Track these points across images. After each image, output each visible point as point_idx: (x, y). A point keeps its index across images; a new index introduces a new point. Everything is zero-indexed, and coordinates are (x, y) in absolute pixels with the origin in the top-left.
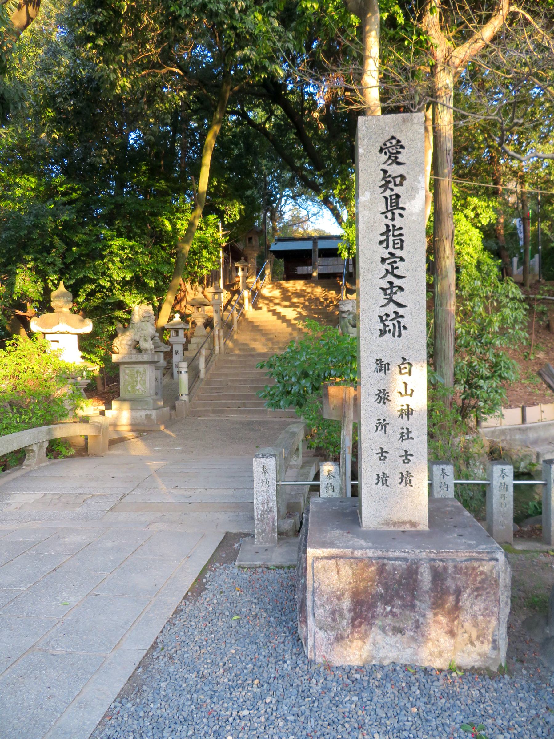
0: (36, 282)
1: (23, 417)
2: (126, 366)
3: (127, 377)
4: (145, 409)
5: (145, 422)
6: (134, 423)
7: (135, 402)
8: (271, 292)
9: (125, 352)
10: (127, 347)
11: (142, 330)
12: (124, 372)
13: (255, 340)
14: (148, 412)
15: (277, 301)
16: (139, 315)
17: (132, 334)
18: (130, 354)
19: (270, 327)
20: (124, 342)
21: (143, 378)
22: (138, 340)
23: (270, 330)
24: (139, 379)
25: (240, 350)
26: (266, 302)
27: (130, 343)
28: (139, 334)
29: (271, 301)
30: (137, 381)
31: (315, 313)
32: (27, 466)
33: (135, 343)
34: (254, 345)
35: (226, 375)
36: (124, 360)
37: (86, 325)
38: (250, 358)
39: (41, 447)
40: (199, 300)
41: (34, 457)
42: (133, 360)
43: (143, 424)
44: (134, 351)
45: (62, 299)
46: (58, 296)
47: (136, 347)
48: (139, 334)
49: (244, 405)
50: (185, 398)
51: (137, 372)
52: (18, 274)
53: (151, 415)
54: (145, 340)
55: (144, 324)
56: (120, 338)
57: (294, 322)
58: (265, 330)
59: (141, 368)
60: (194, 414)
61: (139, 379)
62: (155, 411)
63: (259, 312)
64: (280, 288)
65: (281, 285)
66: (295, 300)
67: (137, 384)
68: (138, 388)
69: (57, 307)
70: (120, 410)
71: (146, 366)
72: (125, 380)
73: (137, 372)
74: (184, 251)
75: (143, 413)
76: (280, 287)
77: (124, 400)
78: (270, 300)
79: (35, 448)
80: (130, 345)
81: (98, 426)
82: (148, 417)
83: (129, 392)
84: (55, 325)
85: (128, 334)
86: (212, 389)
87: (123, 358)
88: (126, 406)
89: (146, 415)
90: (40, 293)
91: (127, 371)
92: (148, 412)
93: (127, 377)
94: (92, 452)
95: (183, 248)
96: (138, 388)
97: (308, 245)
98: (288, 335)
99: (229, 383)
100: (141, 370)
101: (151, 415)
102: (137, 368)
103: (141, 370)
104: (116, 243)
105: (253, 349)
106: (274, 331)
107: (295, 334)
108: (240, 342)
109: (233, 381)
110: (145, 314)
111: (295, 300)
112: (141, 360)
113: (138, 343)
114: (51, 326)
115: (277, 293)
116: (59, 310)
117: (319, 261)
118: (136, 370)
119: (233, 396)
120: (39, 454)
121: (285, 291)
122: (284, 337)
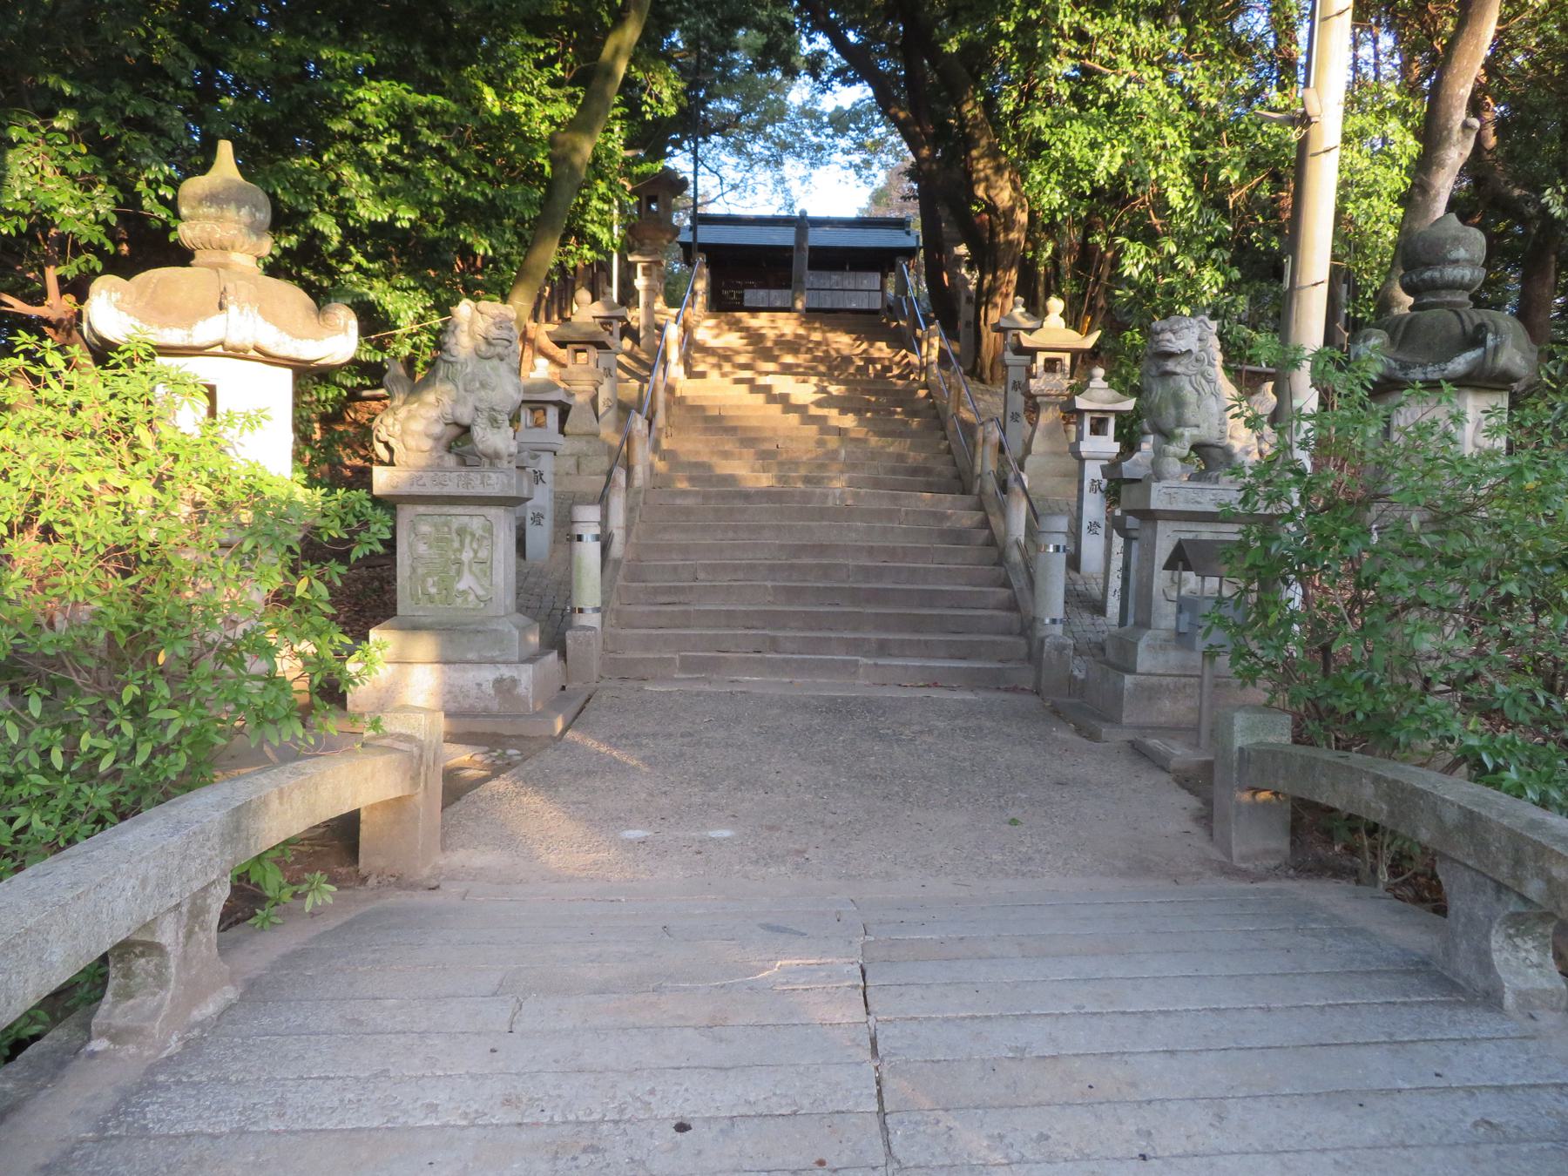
0: (88, 186)
1: (86, 741)
2: (421, 509)
3: (422, 548)
4: (493, 662)
5: (495, 706)
6: (453, 707)
7: (457, 636)
8: (717, 336)
9: (422, 460)
10: (427, 444)
11: (483, 386)
12: (413, 528)
13: (726, 455)
14: (506, 672)
15: (742, 359)
16: (472, 335)
17: (446, 399)
18: (437, 467)
19: (754, 423)
20: (417, 426)
21: (483, 554)
22: (466, 420)
23: (758, 429)
24: (467, 556)
25: (691, 479)
26: (713, 360)
27: (437, 429)
28: (471, 400)
29: (727, 358)
30: (459, 563)
31: (869, 392)
32: (117, 1036)
33: (455, 431)
34: (726, 467)
35: (685, 550)
36: (416, 490)
37: (335, 330)
38: (738, 504)
39: (198, 912)
40: (585, 329)
41: (161, 981)
42: (452, 489)
43: (487, 714)
44: (450, 460)
45: (231, 212)
46: (213, 198)
47: (458, 440)
48: (471, 400)
49: (774, 644)
50: (591, 619)
51: (461, 532)
52: (12, 145)
53: (514, 682)
54: (494, 422)
55: (488, 365)
56: (402, 413)
57: (814, 411)
58: (745, 429)
59: (474, 519)
60: (622, 671)
61: (467, 556)
62: (529, 668)
63: (697, 382)
64: (740, 330)
65: (739, 321)
66: (789, 359)
67: (459, 573)
68: (462, 586)
69: (209, 245)
70: (401, 661)
71: (493, 512)
72: (416, 559)
73: (461, 532)
74: (577, 160)
75: (488, 675)
76: (736, 326)
77: (414, 627)
78: (724, 356)
79: (168, 936)
80: (437, 439)
81: (411, 756)
82: (504, 688)
83: (431, 599)
84: (204, 314)
85: (430, 397)
86: (656, 591)
87: (413, 481)
88: (424, 647)
89: (499, 682)
90: (105, 223)
91: (425, 528)
92: (506, 672)
93: (422, 548)
94: (380, 862)
95: (575, 149)
96: (462, 586)
97: (784, 237)
98: (811, 445)
99: (701, 575)
100: (476, 524)
101: (514, 682)
102: (461, 517)
103: (476, 524)
104: (373, 97)
105: (730, 479)
106: (767, 434)
107: (833, 442)
108: (684, 458)
109: (712, 569)
110: (494, 332)
111: (789, 359)
112: (478, 490)
113: (466, 430)
114: (189, 318)
115: (733, 339)
116: (216, 257)
117: (811, 278)
118: (456, 523)
119: (730, 614)
120: (185, 959)
121: (755, 337)
122: (808, 451)
